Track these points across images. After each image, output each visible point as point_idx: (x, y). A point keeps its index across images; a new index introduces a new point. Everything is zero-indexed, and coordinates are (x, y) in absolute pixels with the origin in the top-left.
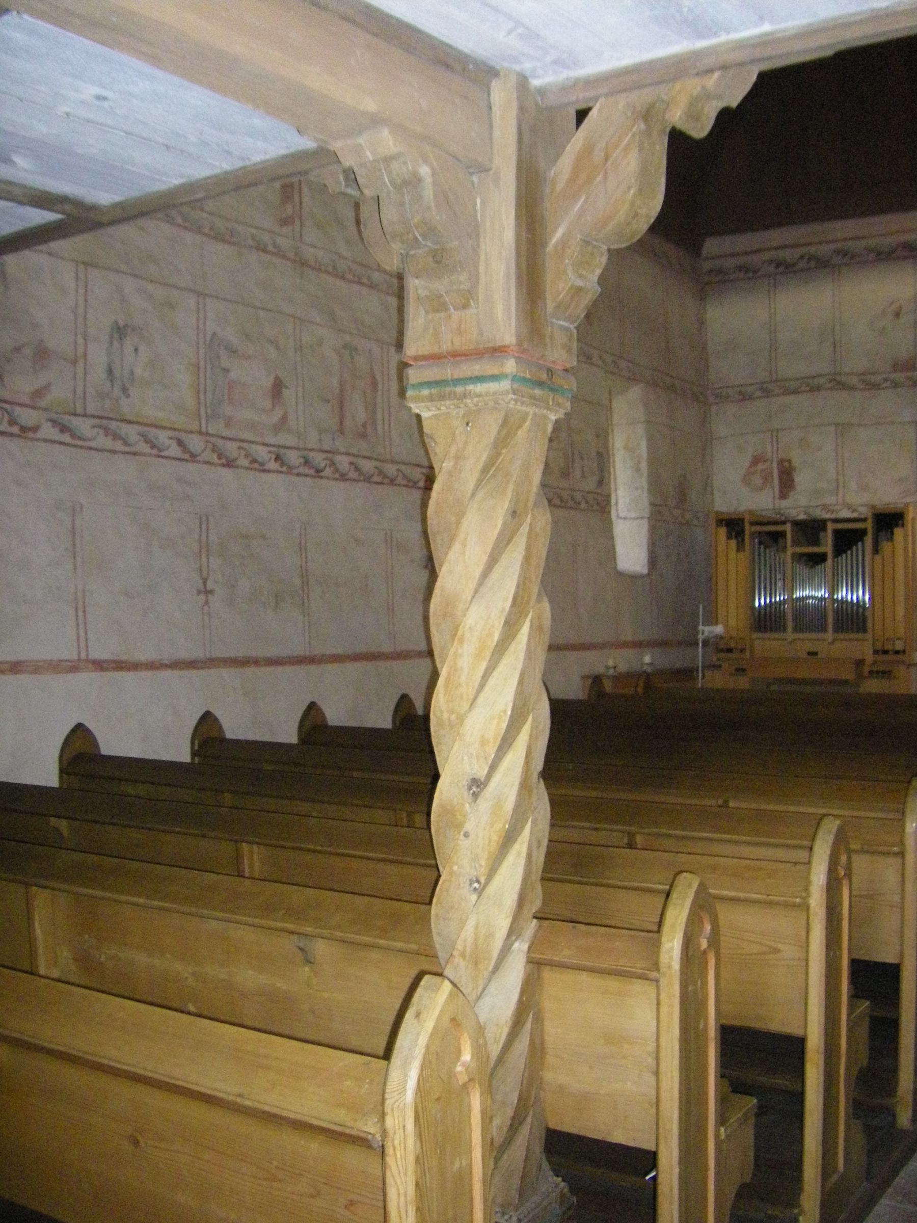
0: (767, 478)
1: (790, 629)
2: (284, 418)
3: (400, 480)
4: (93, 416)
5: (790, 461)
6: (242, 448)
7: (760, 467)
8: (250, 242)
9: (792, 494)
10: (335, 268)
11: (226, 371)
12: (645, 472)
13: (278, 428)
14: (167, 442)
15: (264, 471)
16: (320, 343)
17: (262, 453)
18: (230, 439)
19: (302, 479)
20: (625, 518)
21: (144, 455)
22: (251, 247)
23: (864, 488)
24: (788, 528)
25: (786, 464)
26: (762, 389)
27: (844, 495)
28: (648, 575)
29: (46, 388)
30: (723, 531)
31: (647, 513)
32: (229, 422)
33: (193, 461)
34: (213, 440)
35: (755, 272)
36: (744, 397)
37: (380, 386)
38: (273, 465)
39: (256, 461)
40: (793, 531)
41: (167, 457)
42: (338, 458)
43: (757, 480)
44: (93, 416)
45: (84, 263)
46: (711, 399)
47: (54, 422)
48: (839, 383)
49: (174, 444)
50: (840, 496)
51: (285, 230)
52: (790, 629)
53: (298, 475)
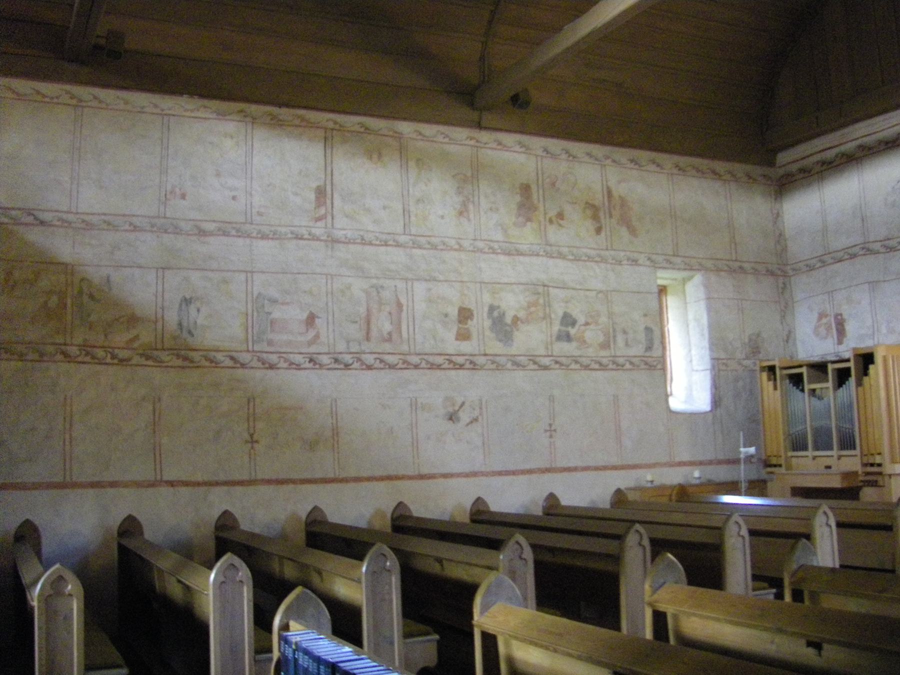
0: (829, 328)
1: (835, 446)
2: (317, 336)
3: (423, 365)
4: (168, 349)
5: (841, 315)
6: (282, 357)
7: (824, 321)
8: (290, 236)
9: (845, 339)
10: (363, 239)
11: (270, 313)
12: (707, 336)
13: (310, 343)
14: (222, 359)
15: (299, 369)
16: (349, 287)
17: (298, 359)
18: (271, 353)
19: (331, 372)
20: (697, 371)
21: (204, 367)
22: (291, 238)
23: (891, 331)
24: (804, 370)
25: (839, 317)
26: (820, 261)
27: (878, 338)
28: (711, 411)
29: (137, 337)
30: (765, 375)
31: (709, 366)
32: (270, 343)
33: (243, 368)
34: (258, 354)
35: (809, 172)
36: (811, 268)
37: (405, 308)
38: (308, 365)
39: (293, 364)
40: (808, 373)
41: (223, 367)
42: (364, 357)
43: (823, 331)
44: (168, 349)
45: (162, 268)
46: (791, 273)
47: (142, 355)
48: (868, 250)
49: (228, 359)
50: (876, 339)
51: (319, 224)
52: (835, 446)
53: (329, 369)
